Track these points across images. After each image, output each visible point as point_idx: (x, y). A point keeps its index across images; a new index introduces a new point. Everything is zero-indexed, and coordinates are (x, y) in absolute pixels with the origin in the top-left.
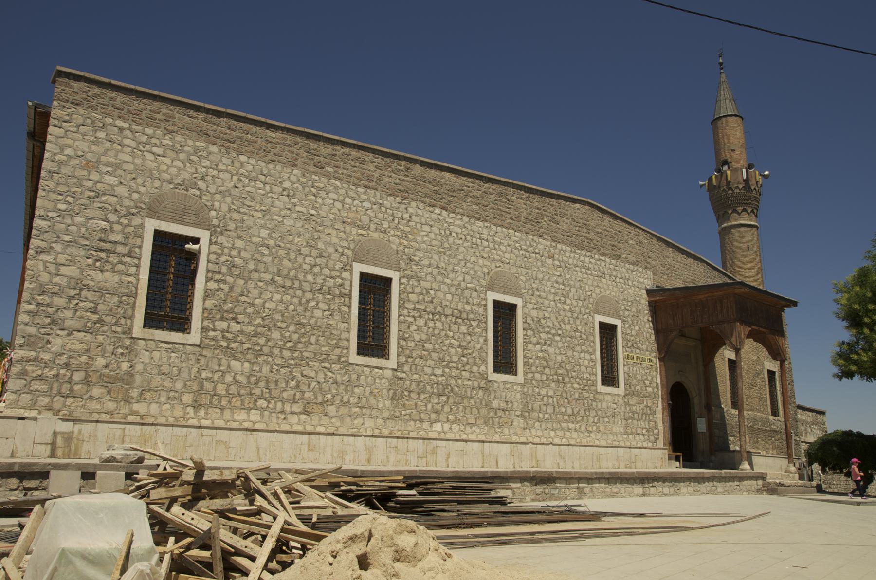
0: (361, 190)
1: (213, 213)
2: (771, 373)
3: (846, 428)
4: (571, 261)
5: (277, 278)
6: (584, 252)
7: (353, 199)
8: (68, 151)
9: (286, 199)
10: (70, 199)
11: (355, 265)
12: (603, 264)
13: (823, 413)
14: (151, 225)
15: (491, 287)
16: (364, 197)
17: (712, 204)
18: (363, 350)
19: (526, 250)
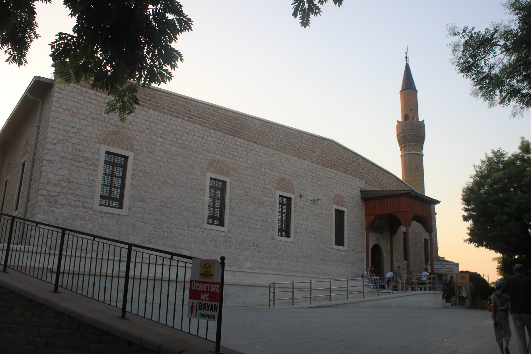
0: (212, 131)
1: (135, 142)
2: (426, 240)
3: (426, 138)
4: (321, 174)
5: (168, 180)
6: (328, 169)
7: (208, 136)
8: (64, 107)
9: (173, 135)
10: (64, 134)
11: (208, 173)
12: (338, 176)
13: (100, 205)
14: (104, 148)
15: (277, 188)
16: (214, 135)
17: (398, 140)
18: (337, 243)
19: (298, 168)
